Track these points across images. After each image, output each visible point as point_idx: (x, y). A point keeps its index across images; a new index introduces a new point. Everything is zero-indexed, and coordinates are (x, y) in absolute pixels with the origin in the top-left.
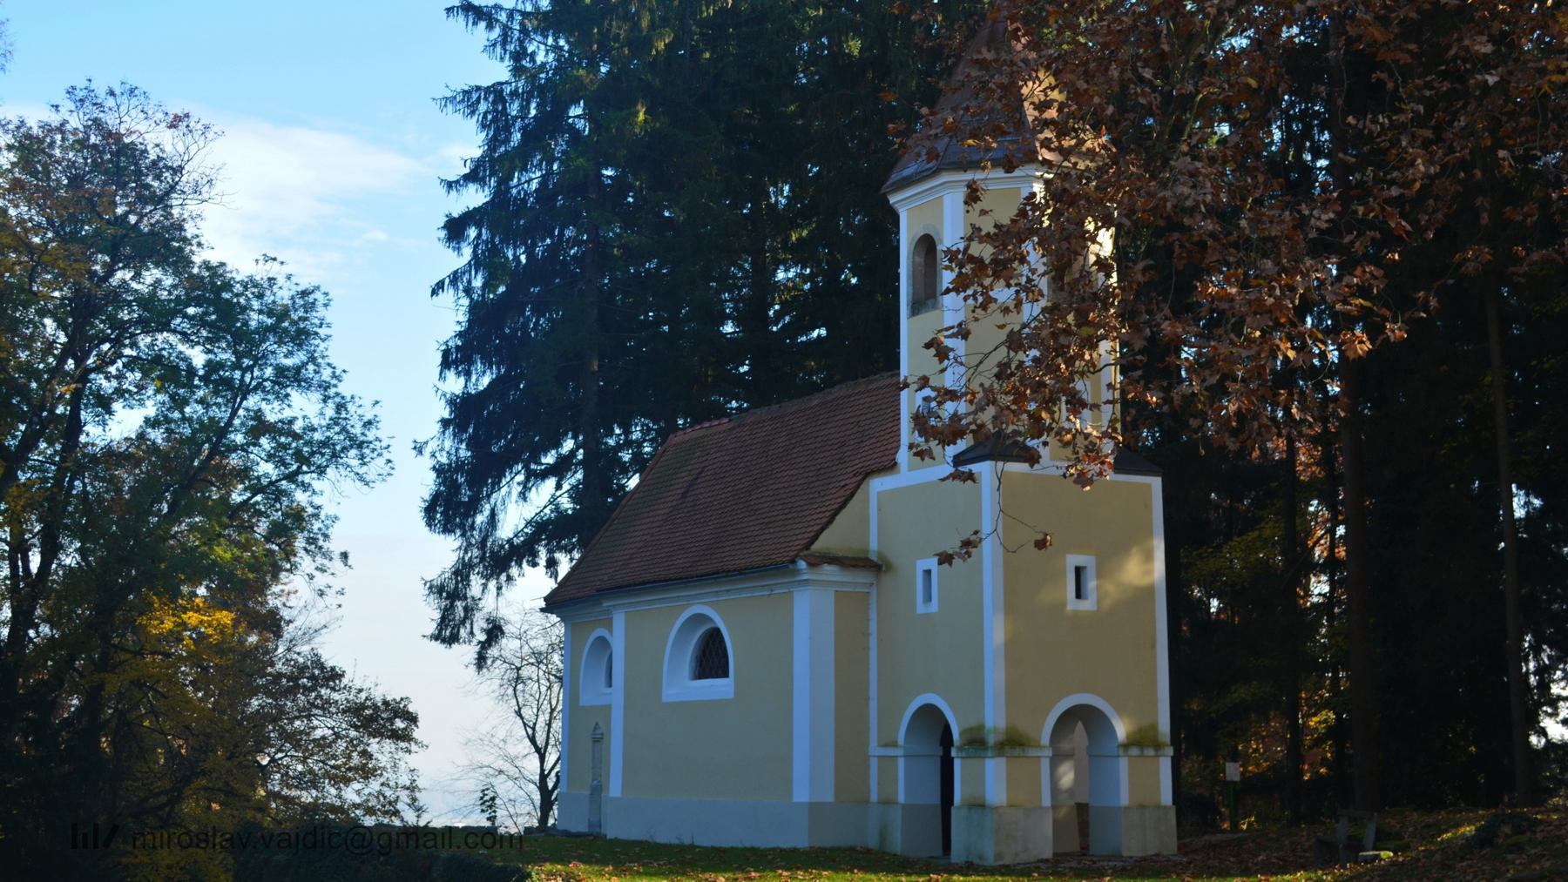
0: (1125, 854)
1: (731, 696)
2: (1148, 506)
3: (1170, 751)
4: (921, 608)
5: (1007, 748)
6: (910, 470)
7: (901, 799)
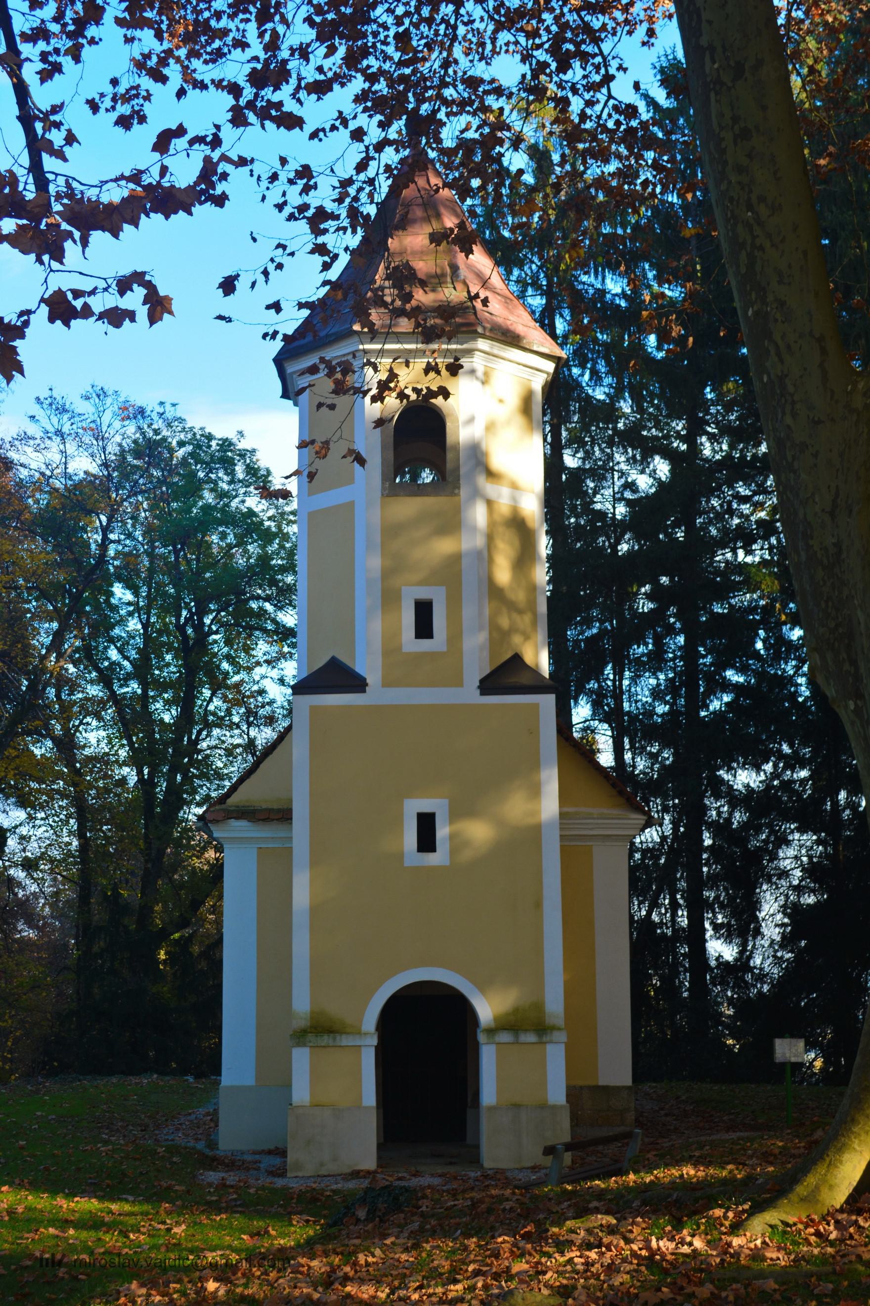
2: (533, 732)
6: (352, 503)
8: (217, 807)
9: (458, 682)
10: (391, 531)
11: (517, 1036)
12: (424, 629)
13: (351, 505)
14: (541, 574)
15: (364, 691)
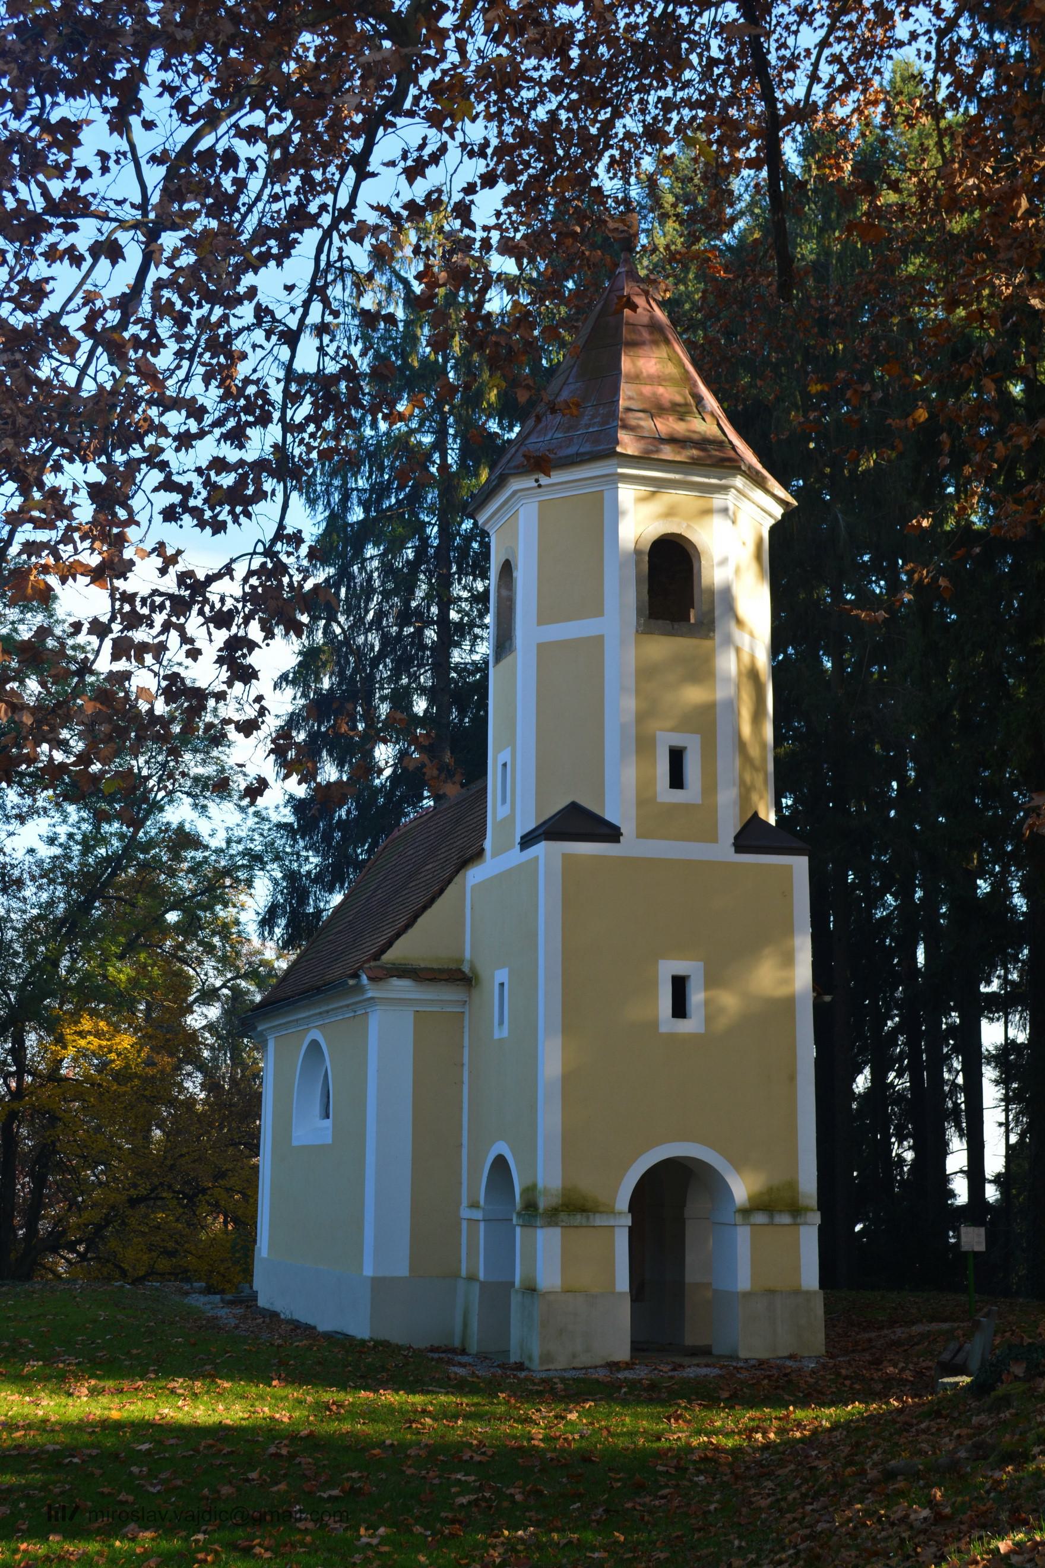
0: (743, 1354)
1: (329, 1140)
2: (787, 894)
3: (816, 1218)
4: (496, 1036)
5: (563, 1216)
7: (481, 1276)
8: (372, 964)
9: (713, 838)
10: (646, 673)
11: (771, 1217)
12: (677, 780)
13: (598, 641)
14: (769, 731)
15: (618, 841)
